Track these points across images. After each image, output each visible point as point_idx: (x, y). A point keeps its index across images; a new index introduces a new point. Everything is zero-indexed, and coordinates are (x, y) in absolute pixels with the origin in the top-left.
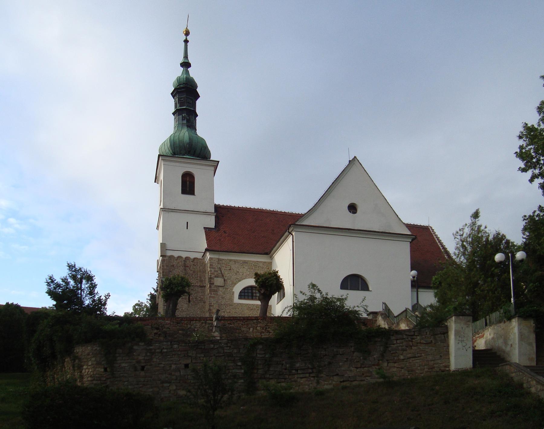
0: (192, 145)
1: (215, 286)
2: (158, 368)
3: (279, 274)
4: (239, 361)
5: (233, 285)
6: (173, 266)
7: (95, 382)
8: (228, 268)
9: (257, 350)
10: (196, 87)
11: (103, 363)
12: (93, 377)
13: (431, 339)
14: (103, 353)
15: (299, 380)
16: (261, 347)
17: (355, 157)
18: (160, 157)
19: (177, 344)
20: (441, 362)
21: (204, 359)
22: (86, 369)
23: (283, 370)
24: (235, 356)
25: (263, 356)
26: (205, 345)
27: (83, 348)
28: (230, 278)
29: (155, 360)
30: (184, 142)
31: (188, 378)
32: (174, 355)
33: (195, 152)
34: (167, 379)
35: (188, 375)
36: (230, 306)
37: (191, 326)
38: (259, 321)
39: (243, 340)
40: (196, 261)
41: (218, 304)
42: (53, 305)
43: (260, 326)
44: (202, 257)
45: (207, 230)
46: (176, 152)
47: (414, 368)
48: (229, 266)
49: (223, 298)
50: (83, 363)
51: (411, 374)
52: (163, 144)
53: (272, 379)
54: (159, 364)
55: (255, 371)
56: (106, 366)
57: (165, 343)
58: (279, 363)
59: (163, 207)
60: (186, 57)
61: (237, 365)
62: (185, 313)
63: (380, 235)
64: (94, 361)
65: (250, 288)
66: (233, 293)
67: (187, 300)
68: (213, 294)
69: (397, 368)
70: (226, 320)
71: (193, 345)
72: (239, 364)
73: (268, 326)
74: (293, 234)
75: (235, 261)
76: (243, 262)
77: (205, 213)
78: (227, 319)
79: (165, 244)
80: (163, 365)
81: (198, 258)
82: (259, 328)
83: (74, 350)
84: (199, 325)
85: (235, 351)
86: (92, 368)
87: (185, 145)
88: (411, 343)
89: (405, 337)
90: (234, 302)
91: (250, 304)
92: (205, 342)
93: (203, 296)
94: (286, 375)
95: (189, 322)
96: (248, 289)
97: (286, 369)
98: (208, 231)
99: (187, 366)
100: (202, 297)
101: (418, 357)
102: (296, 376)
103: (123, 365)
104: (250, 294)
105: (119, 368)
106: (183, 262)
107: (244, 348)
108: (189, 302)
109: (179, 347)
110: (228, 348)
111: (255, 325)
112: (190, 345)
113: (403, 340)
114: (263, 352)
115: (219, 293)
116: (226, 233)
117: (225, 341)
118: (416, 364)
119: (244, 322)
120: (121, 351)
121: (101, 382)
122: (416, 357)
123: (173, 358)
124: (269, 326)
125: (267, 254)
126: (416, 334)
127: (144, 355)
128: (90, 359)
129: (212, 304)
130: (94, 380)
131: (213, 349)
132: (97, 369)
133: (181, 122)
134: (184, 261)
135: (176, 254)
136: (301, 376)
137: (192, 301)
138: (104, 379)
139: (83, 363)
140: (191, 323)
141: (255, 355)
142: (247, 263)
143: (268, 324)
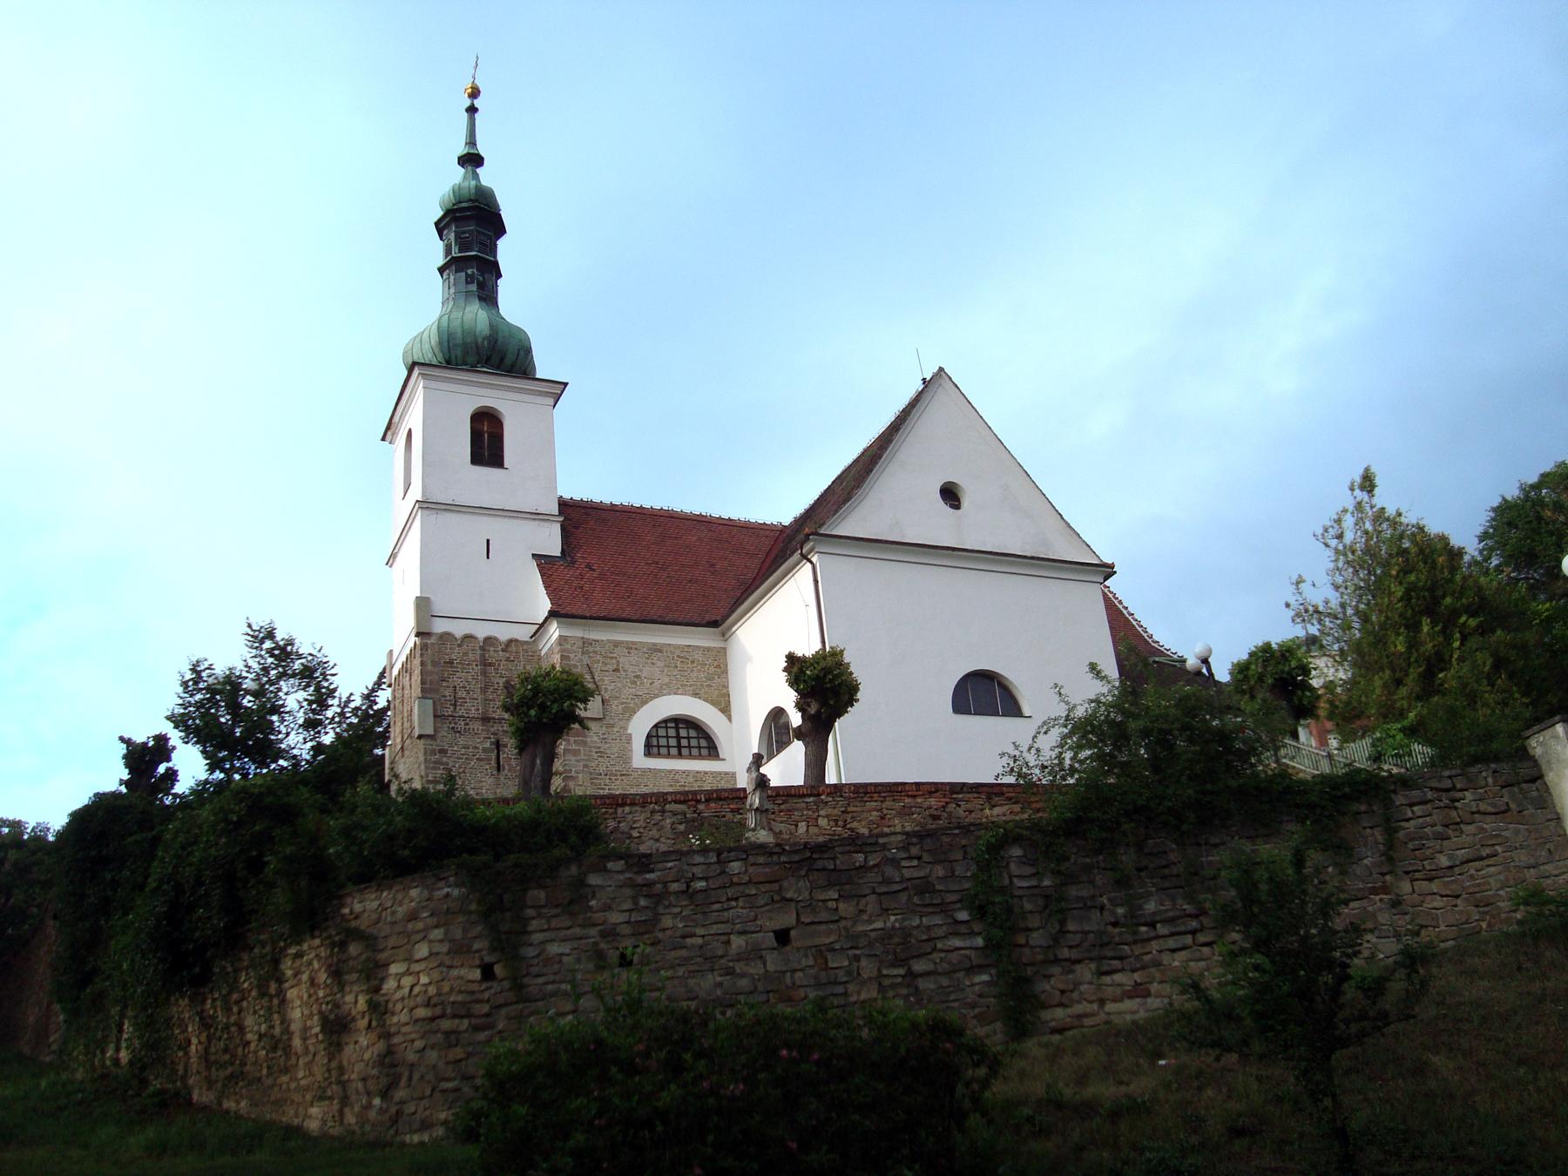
0: (496, 341)
2: (684, 953)
3: (847, 658)
4: (959, 905)
5: (628, 715)
6: (451, 662)
7: (446, 1024)
8: (611, 668)
9: (1008, 863)
11: (476, 946)
12: (435, 1005)
13: (1505, 799)
14: (473, 907)
15: (1166, 958)
16: (1016, 852)
17: (941, 369)
18: (416, 368)
19: (743, 859)
20: (1556, 872)
21: (841, 905)
22: (399, 976)
23: (1110, 928)
24: (941, 891)
25: (1034, 883)
26: (834, 859)
27: (385, 894)
28: (617, 695)
29: (667, 922)
30: (478, 333)
31: (794, 984)
32: (732, 899)
33: (502, 359)
34: (719, 992)
35: (794, 971)
37: (619, 822)
38: (823, 797)
39: (957, 831)
40: (513, 648)
41: (591, 774)
42: (121, 780)
43: (827, 816)
44: (531, 637)
45: (544, 563)
46: (453, 358)
47: (1489, 893)
48: (614, 661)
49: (601, 754)
50: (382, 956)
51: (1486, 913)
52: (418, 340)
53: (1079, 961)
54: (684, 937)
55: (1021, 940)
56: (488, 959)
57: (698, 859)
58: (1089, 904)
59: (423, 495)
60: (472, 141)
61: (957, 922)
63: (1027, 565)
64: (441, 941)
65: (673, 725)
66: (629, 738)
67: (493, 763)
68: (575, 741)
69: (1442, 896)
70: (726, 799)
71: (796, 858)
72: (963, 916)
73: (848, 813)
74: (814, 559)
75: (630, 647)
76: (650, 649)
77: (536, 516)
78: (726, 795)
79: (428, 599)
80: (700, 941)
81: (520, 639)
82: (823, 822)
83: (343, 905)
84: (642, 817)
85: (940, 871)
86: (431, 969)
87: (480, 340)
88: (1454, 814)
89: (1430, 795)
91: (677, 772)
92: (834, 847)
94: (1122, 944)
95: (611, 811)
96: (667, 727)
97: (1115, 924)
98: (546, 563)
99: (782, 937)
101: (1489, 856)
102: (1153, 943)
103: (554, 949)
104: (673, 742)
105: (537, 965)
106: (479, 652)
107: (964, 858)
108: (499, 770)
109: (746, 871)
110: (915, 863)
111: (810, 813)
112: (783, 859)
113: (1429, 806)
114: (1029, 870)
115: (589, 740)
116: (594, 570)
117: (900, 838)
118: (1491, 880)
119: (779, 805)
120: (542, 895)
121: (474, 1021)
122: (1481, 859)
123: (731, 911)
124: (855, 814)
125: (714, 624)
126: (1458, 786)
127: (628, 905)
128: (420, 936)
129: (573, 774)
130: (443, 1016)
131: (864, 868)
132: (455, 972)
133: (462, 286)
134: (482, 648)
135: (459, 629)
136: (1171, 943)
137: (507, 767)
138: (486, 1008)
139: (382, 956)
140: (616, 813)
141: (1006, 882)
142: (661, 651)
143: (849, 809)
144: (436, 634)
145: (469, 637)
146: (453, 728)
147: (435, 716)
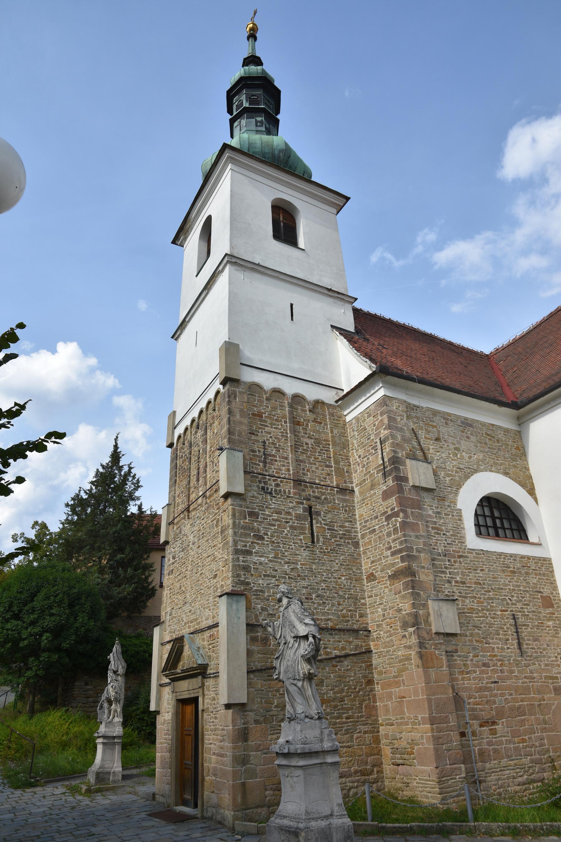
1: (414, 487)
6: (260, 415)
10: (274, 81)
36: (461, 560)
40: (319, 410)
44: (337, 402)
62: (305, 583)
75: (447, 418)
76: (463, 423)
87: (276, 152)
90: (469, 547)
91: (506, 555)
93: (351, 522)
100: (347, 524)
104: (489, 522)
108: (313, 542)
125: (515, 406)
129: (415, 553)
144: (245, 383)
145: (278, 392)
146: (263, 488)
147: (245, 472)
